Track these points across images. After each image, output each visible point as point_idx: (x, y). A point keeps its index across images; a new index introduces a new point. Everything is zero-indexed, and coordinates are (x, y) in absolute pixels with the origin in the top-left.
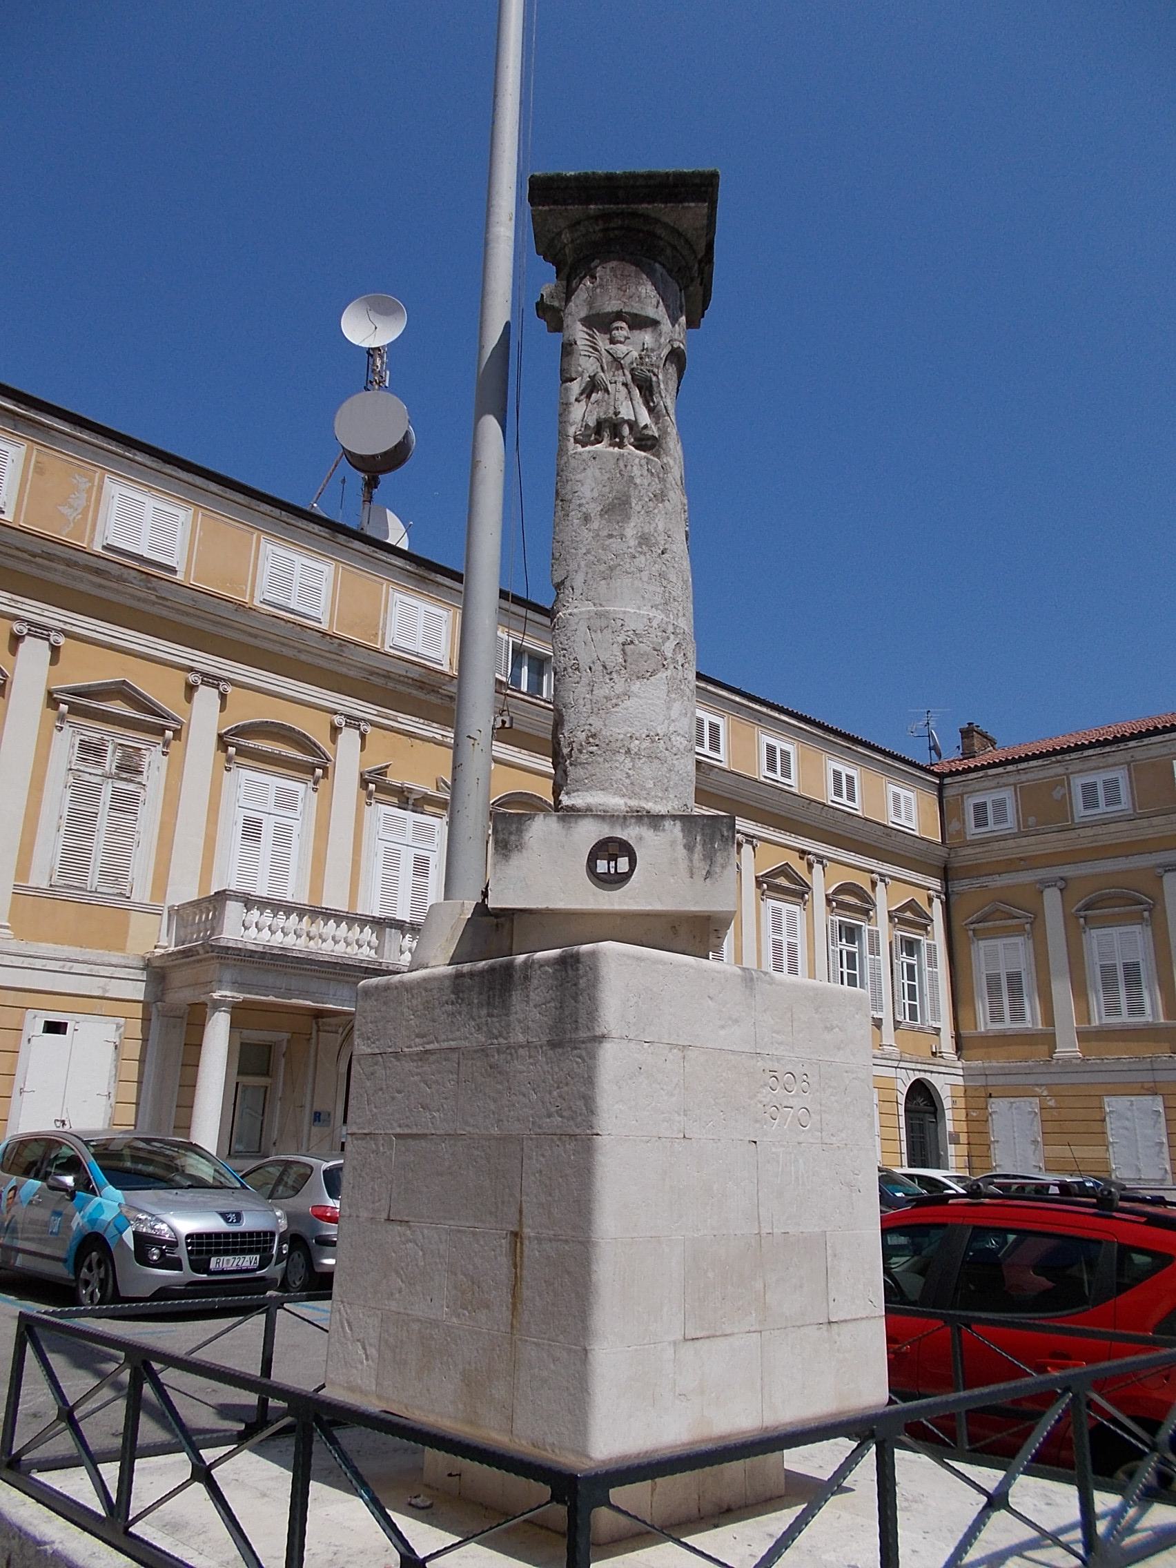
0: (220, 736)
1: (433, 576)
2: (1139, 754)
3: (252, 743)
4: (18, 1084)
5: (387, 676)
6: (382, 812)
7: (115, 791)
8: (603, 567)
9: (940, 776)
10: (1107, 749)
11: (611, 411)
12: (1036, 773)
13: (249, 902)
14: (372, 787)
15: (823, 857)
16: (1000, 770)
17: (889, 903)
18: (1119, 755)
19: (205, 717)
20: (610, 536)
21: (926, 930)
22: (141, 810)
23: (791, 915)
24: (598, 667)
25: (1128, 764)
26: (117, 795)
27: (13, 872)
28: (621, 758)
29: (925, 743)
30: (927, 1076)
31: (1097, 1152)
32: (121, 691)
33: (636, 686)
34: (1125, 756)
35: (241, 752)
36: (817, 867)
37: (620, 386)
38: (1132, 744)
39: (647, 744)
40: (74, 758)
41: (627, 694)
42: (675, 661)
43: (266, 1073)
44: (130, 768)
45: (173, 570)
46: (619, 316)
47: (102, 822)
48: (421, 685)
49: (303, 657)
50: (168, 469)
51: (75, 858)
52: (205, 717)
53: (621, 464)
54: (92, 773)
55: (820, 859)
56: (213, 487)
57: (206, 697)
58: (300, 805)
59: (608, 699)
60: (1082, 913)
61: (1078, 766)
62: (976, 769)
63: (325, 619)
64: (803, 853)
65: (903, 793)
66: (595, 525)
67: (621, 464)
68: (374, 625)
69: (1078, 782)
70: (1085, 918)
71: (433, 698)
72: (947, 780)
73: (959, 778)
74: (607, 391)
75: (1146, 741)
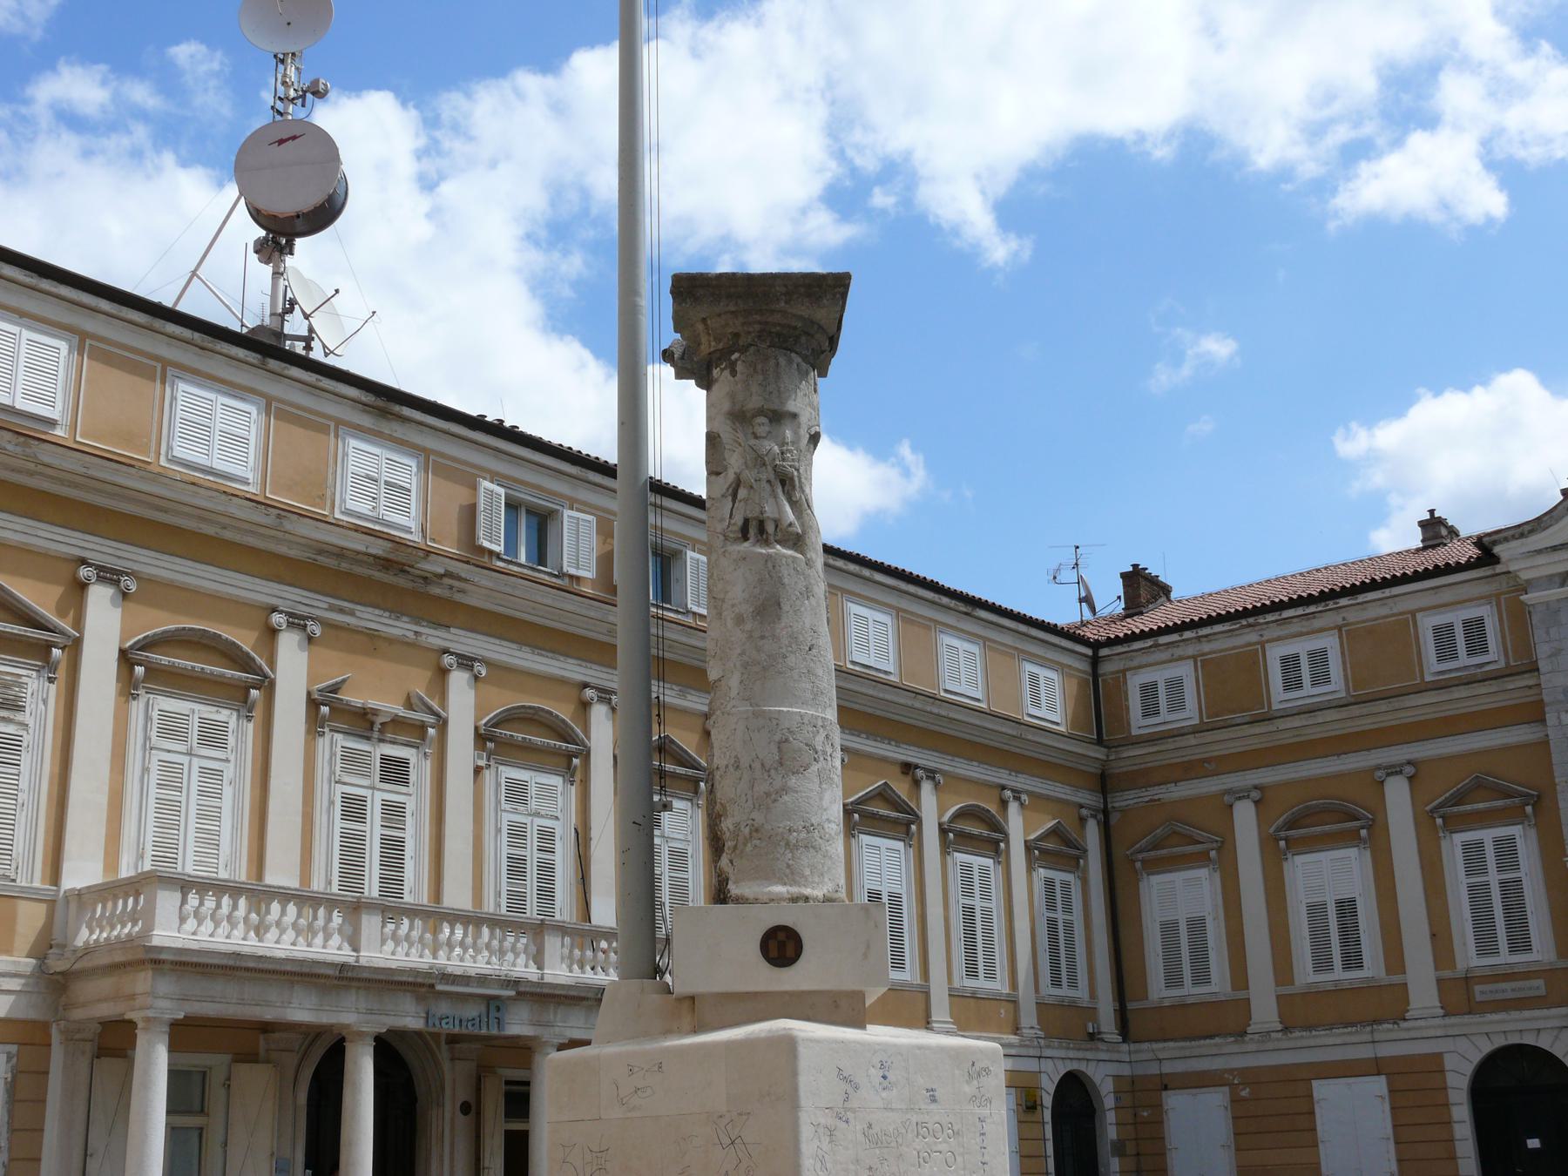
0: (123, 653)
1: (397, 408)
2: (1353, 616)
5: (341, 553)
6: (335, 743)
9: (1096, 645)
10: (1312, 609)
11: (758, 509)
12: (1223, 642)
13: (185, 885)
14: (325, 710)
16: (1175, 637)
17: (1026, 832)
18: (1329, 617)
19: (105, 623)
20: (763, 637)
22: (25, 760)
23: (984, 871)
24: (757, 765)
25: (1339, 628)
29: (1073, 593)
30: (1082, 1067)
33: (793, 781)
34: (1336, 618)
35: (154, 672)
36: (927, 788)
37: (764, 484)
38: (1344, 602)
39: (803, 835)
41: (785, 790)
42: (825, 753)
43: (202, 1111)
45: (52, 423)
46: (761, 412)
48: (385, 563)
49: (228, 535)
50: (46, 284)
52: (105, 623)
53: (770, 565)
55: (931, 774)
56: (105, 305)
57: (99, 597)
58: (231, 740)
59: (768, 794)
60: (1283, 834)
61: (1275, 631)
62: (1143, 635)
63: (413, 525)
64: (907, 768)
65: (1043, 673)
66: (748, 627)
67: (770, 565)
68: (320, 483)
69: (1275, 653)
70: (1286, 839)
71: (401, 581)
72: (1104, 652)
73: (1119, 649)
75: (1361, 598)
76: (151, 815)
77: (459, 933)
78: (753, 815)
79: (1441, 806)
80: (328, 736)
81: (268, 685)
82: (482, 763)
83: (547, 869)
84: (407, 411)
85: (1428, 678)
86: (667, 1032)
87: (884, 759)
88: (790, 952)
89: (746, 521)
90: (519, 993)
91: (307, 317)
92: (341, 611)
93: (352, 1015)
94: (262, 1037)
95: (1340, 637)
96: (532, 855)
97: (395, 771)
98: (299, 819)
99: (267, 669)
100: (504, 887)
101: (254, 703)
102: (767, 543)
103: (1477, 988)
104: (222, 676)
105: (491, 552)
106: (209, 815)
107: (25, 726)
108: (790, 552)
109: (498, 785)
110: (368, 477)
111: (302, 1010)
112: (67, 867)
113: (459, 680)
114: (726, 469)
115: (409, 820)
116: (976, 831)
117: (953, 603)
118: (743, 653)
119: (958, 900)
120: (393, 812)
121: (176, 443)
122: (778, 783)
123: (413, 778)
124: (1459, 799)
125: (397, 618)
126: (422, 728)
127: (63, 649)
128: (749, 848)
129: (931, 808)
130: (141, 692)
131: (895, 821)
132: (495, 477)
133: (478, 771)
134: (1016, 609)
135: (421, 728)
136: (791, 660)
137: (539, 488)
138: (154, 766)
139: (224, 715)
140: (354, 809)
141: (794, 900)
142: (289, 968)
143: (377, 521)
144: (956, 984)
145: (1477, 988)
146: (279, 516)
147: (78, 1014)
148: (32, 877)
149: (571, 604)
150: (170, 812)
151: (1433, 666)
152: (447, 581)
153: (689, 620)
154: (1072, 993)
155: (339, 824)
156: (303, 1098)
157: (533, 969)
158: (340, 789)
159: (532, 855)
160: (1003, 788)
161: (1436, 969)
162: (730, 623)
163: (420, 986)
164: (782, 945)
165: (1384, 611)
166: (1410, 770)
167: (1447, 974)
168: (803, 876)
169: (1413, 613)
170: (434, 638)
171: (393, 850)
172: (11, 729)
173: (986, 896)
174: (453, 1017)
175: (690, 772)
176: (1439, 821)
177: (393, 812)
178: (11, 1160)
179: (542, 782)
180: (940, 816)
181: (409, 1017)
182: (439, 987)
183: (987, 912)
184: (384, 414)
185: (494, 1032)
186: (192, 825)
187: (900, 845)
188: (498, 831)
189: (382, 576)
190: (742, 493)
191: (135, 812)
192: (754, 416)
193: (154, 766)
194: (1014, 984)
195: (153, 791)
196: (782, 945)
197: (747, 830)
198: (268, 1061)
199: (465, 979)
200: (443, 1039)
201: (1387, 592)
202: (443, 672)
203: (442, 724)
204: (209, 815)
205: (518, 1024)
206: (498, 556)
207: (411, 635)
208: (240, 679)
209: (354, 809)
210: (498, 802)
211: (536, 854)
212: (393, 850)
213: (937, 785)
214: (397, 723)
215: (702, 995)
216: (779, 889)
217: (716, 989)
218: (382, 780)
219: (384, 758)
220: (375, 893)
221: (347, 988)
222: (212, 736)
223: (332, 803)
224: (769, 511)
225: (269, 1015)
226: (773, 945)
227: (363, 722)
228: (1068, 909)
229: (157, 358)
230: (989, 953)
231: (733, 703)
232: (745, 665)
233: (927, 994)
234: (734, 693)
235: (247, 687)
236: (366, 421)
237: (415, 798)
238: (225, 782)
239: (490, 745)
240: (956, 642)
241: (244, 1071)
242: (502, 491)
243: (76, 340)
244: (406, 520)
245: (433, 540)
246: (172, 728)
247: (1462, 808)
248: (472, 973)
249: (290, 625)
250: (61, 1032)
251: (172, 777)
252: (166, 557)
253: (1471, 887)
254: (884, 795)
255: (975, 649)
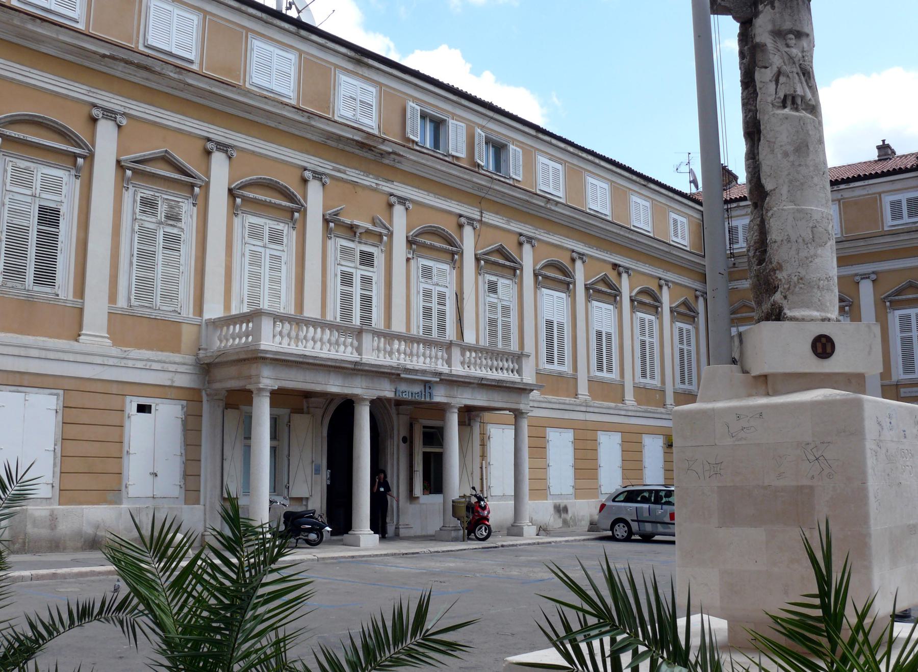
2: (847, 194)
3: (148, 168)
4: (126, 448)
5: (339, 138)
7: (166, 234)
8: (797, 184)
11: (792, 90)
14: (332, 225)
15: (583, 255)
17: (671, 303)
19: (220, 174)
20: (800, 165)
21: (615, 300)
22: (183, 248)
23: (650, 322)
24: (800, 240)
25: (839, 201)
26: (168, 238)
27: (107, 298)
28: (815, 290)
31: (428, 450)
32: (166, 160)
33: (819, 251)
36: (624, 276)
38: (842, 186)
39: (826, 282)
40: (137, 211)
41: (816, 255)
44: (173, 217)
45: (191, 62)
46: (791, 32)
47: (159, 258)
48: (362, 145)
51: (145, 286)
54: (149, 222)
55: (627, 270)
59: (807, 258)
64: (615, 266)
65: (680, 219)
66: (791, 159)
68: (239, 64)
70: (890, 302)
71: (369, 155)
74: (788, 76)
75: (852, 185)
76: (246, 280)
77: (403, 347)
78: (799, 270)
79: (889, 296)
80: (333, 239)
81: (303, 210)
82: (410, 256)
83: (442, 314)
84: (371, 62)
85: (886, 229)
86: (750, 395)
87: (605, 261)
88: (829, 350)
89: (785, 96)
90: (441, 380)
91: (299, 12)
92: (339, 171)
93: (357, 388)
94: (304, 400)
95: (839, 205)
96: (435, 307)
97: (367, 259)
98: (320, 284)
99: (302, 201)
100: (421, 324)
101: (296, 220)
102: (797, 109)
103: (902, 390)
104: (280, 205)
105: (413, 141)
106: (275, 281)
107: (182, 230)
108: (810, 116)
109: (418, 268)
110: (351, 97)
111: (335, 386)
112: (205, 307)
113: (399, 210)
114: (771, 65)
115: (374, 286)
116: (647, 301)
117: (638, 179)
118: (789, 174)
119: (638, 337)
120: (366, 281)
121: (254, 75)
122: (812, 252)
123: (376, 263)
124: (899, 292)
125: (367, 176)
126: (380, 235)
127: (200, 187)
128: (797, 289)
129: (626, 287)
130: (239, 212)
131: (609, 294)
132: (415, 99)
133: (408, 260)
134: (668, 184)
135: (380, 236)
136: (816, 180)
137: (437, 107)
138: (247, 253)
139: (281, 226)
140: (347, 279)
141: (823, 320)
142: (329, 363)
143: (356, 121)
144: (636, 381)
145: (902, 390)
146: (309, 118)
147: (217, 386)
148: (188, 312)
149: (455, 171)
150: (255, 278)
151: (889, 222)
152: (393, 156)
153: (511, 182)
154: (690, 387)
155: (339, 287)
156: (325, 434)
157: (446, 367)
158: (340, 268)
159: (435, 307)
160: (660, 279)
161: (882, 379)
162: (779, 156)
163: (393, 375)
164: (824, 347)
165: (864, 192)
166: (874, 277)
167: (887, 382)
168: (826, 306)
169: (880, 194)
170: (386, 187)
171: (366, 301)
172: (175, 231)
173: (651, 336)
174: (409, 392)
175: (512, 264)
176: (888, 304)
177: (366, 281)
178: (187, 460)
179: (440, 267)
180: (631, 292)
181: (387, 391)
182: (402, 376)
183: (651, 344)
184: (359, 62)
185: (428, 400)
186: (267, 286)
187: (611, 307)
188: (418, 292)
189: (364, 150)
190: (782, 79)
191: (238, 277)
192: (786, 34)
193: (247, 253)
194: (663, 382)
195: (247, 267)
196: (824, 347)
197: (796, 279)
198: (308, 413)
199: (415, 371)
200: (393, 402)
201: (867, 182)
202: (391, 206)
203: (390, 235)
204: (275, 281)
205: (440, 396)
206: (417, 143)
207: (374, 185)
208: (289, 207)
209: (347, 279)
210: (418, 277)
211: (437, 306)
212: (366, 301)
213: (629, 275)
214: (368, 232)
215: (775, 375)
216: (816, 314)
217: (781, 370)
218: (361, 264)
219: (362, 252)
220: (358, 323)
221: (356, 375)
222: (276, 238)
223: (336, 275)
224: (799, 92)
225: (318, 388)
226: (819, 345)
227: (351, 230)
228: (689, 344)
229: (243, 27)
230: (652, 365)
231: (784, 203)
232: (791, 182)
233: (623, 386)
234: (784, 197)
235: (292, 209)
236: (350, 66)
237: (377, 273)
238: (283, 263)
239: (414, 246)
240: (639, 200)
241: (296, 418)
242: (418, 108)
243: (201, 16)
244: (371, 123)
245: (384, 134)
246: (255, 233)
247: (900, 297)
248: (417, 368)
249: (314, 178)
250: (207, 395)
251: (256, 260)
252: (250, 138)
253: (902, 339)
254: (605, 280)
255: (648, 204)
